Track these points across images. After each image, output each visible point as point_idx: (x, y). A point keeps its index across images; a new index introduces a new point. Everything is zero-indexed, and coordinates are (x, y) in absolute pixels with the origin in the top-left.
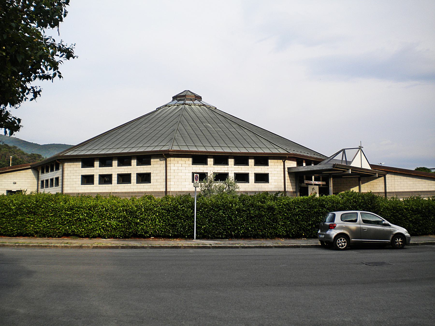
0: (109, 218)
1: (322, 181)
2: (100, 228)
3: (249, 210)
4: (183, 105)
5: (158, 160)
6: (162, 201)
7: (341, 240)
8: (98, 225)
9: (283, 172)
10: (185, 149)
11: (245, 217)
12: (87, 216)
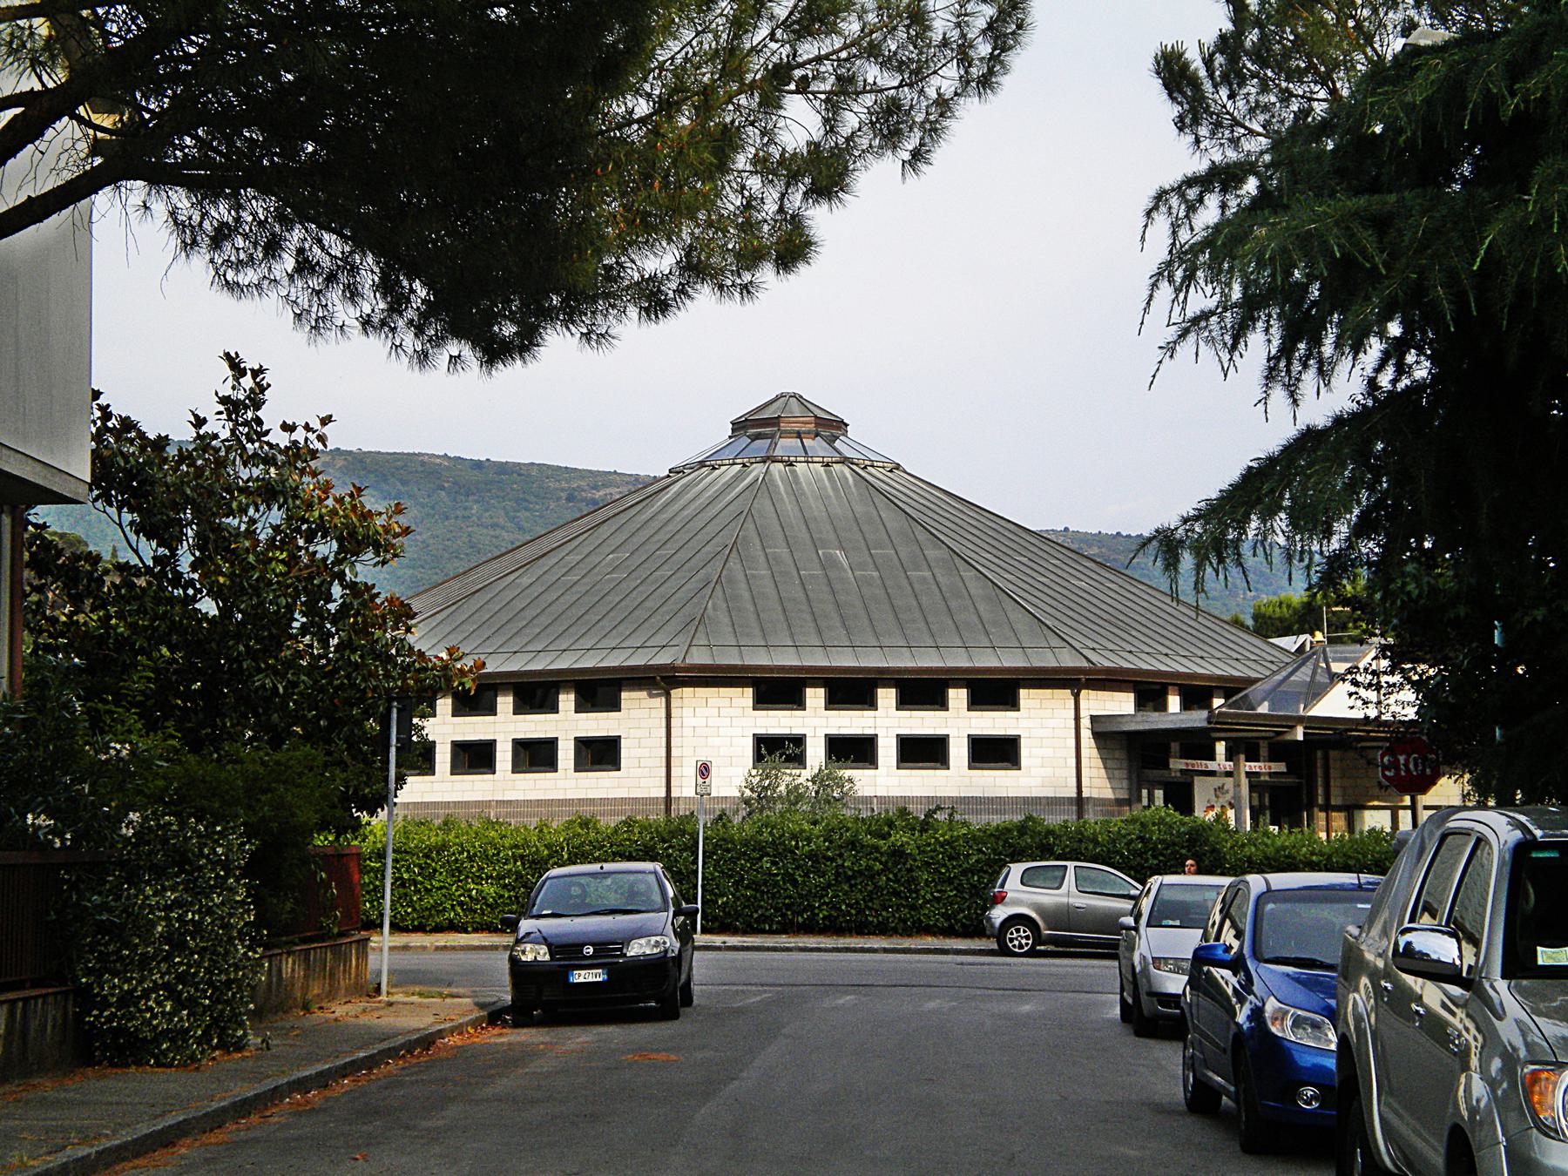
0: (478, 880)
1: (1270, 761)
2: (453, 906)
3: (841, 855)
4: (764, 462)
5: (644, 694)
6: (616, 831)
7: (1018, 931)
8: (449, 897)
9: (1073, 732)
10: (731, 658)
11: (830, 876)
12: (420, 874)
